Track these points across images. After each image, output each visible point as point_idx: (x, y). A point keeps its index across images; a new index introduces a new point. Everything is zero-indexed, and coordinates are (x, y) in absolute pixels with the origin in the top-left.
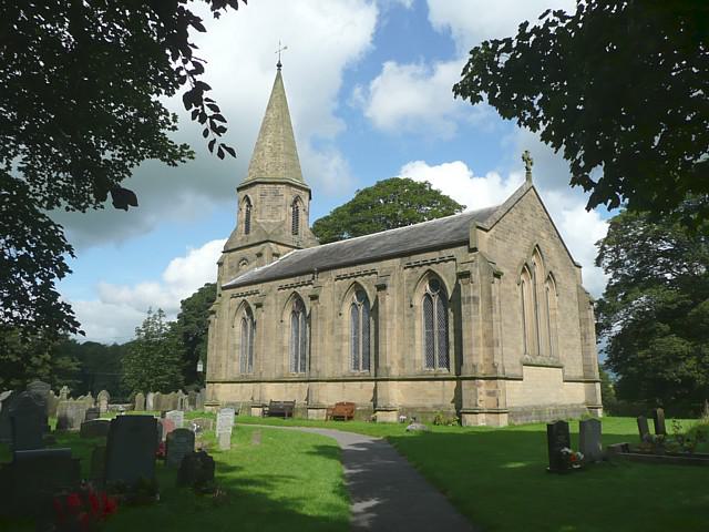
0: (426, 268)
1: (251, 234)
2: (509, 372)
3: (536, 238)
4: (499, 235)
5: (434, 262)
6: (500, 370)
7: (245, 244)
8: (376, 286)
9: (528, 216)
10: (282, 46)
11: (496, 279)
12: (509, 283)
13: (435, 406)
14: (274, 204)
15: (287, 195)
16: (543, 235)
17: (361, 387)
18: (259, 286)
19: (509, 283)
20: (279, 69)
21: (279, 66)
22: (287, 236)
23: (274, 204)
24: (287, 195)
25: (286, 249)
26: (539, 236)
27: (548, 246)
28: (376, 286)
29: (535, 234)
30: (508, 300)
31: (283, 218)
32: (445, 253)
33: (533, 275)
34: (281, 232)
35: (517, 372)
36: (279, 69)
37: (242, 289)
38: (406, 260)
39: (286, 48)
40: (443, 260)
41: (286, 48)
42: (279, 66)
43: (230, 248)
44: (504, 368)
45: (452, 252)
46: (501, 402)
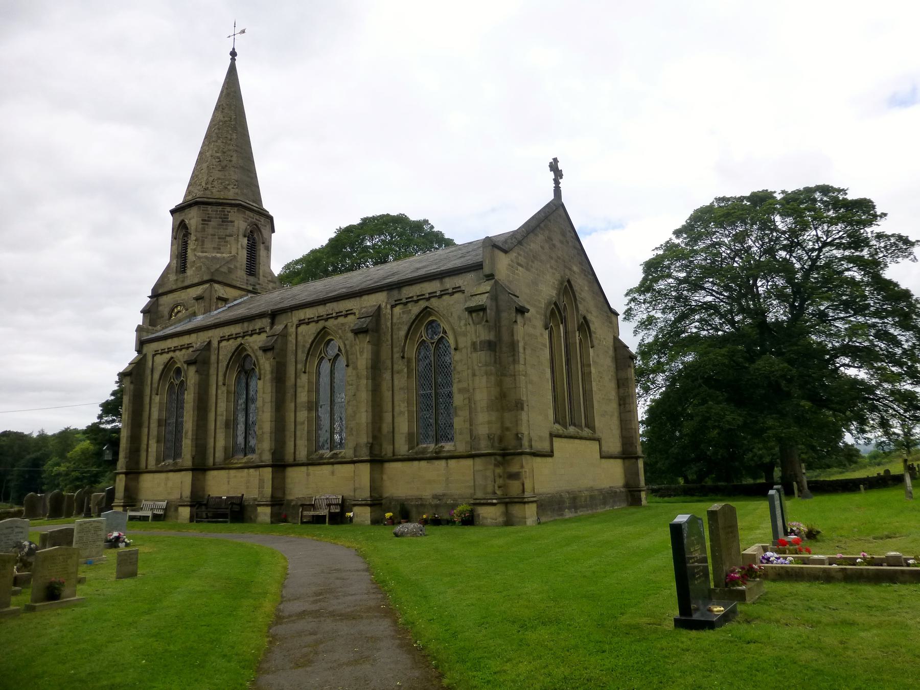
0: (423, 304)
1: (189, 272)
2: (539, 446)
3: (567, 271)
4: (522, 260)
5: (432, 295)
6: (525, 443)
7: (180, 285)
8: (352, 331)
9: (558, 244)
10: (238, 30)
11: (519, 319)
12: (534, 327)
13: (435, 497)
14: (222, 232)
15: (240, 223)
16: (575, 268)
17: (167, 479)
18: (193, 337)
19: (534, 327)
20: (233, 60)
21: (233, 54)
22: (240, 276)
23: (222, 232)
24: (240, 223)
25: (236, 293)
26: (570, 269)
27: (580, 283)
28: (352, 331)
29: (565, 267)
30: (233, 647)
31: (234, 253)
32: (449, 283)
33: (564, 320)
34: (230, 271)
35: (544, 446)
36: (233, 60)
37: (169, 341)
38: (395, 294)
39: (243, 32)
40: (444, 293)
41: (243, 32)
42: (233, 54)
43: (160, 291)
44: (530, 440)
45: (458, 281)
46: (528, 486)
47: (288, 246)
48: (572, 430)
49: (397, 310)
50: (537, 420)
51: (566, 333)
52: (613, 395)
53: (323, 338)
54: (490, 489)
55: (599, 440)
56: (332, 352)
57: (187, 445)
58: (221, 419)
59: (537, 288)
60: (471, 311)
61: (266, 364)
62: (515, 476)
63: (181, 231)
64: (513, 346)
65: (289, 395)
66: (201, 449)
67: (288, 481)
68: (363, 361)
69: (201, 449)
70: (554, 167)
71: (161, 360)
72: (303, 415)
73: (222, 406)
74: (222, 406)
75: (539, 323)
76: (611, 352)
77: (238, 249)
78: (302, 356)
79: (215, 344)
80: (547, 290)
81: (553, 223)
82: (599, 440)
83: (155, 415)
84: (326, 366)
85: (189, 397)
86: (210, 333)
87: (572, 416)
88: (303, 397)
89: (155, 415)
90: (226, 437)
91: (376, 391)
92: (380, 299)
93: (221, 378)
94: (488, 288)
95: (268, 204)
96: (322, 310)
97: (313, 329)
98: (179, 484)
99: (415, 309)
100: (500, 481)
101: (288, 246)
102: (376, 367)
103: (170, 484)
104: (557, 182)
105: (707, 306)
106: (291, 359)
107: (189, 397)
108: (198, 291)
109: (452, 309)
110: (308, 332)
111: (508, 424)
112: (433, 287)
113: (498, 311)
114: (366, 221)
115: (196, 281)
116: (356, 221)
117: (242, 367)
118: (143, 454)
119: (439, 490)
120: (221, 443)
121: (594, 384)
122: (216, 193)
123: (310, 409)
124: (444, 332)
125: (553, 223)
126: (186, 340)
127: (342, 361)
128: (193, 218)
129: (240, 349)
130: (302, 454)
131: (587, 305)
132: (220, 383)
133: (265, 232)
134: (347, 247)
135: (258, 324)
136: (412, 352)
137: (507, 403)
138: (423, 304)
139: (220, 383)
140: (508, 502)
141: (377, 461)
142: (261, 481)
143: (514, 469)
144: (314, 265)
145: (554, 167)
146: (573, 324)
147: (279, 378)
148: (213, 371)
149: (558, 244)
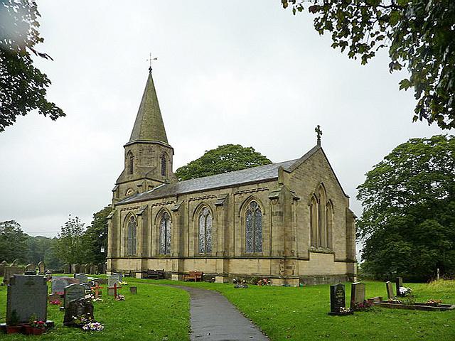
0: (249, 194)
3: (322, 179)
4: (298, 176)
6: (295, 255)
9: (318, 167)
15: (157, 151)
21: (150, 69)
24: (157, 151)
27: (329, 185)
31: (155, 165)
33: (319, 201)
42: (150, 69)
45: (266, 185)
47: (180, 161)
48: (320, 249)
49: (236, 196)
50: (302, 244)
51: (319, 206)
52: (344, 234)
53: (201, 206)
54: (277, 272)
55: (334, 254)
56: (205, 212)
57: (139, 248)
58: (154, 239)
59: (304, 188)
60: (271, 199)
61: (175, 217)
62: (290, 268)
63: (129, 154)
64: (291, 214)
65: (185, 230)
66: (145, 250)
67: (185, 264)
68: (221, 218)
69: (145, 250)
70: (318, 131)
71: (124, 213)
72: (192, 238)
73: (154, 233)
74: (154, 233)
75: (305, 204)
76: (344, 215)
77: (157, 164)
78: (191, 214)
79: (150, 207)
80: (311, 189)
81: (317, 156)
82: (334, 254)
83: (123, 236)
84: (202, 219)
85: (139, 229)
86: (148, 202)
87: (320, 244)
88: (192, 231)
89: (123, 236)
90: (156, 246)
91: (226, 230)
92: (230, 190)
93: (153, 221)
94: (280, 189)
95: (171, 142)
96: (200, 195)
97: (197, 203)
98: (135, 265)
99: (246, 197)
100: (282, 269)
101: (180, 161)
102: (226, 221)
103: (131, 264)
104: (319, 137)
105: (401, 193)
106: (186, 215)
107: (139, 229)
108: (139, 182)
109: (263, 197)
110: (194, 204)
111: (287, 246)
112: (255, 187)
113: (285, 199)
114: (220, 148)
115: (139, 177)
116: (215, 147)
117: (163, 217)
118: (118, 251)
119: (255, 272)
120: (154, 248)
121: (333, 229)
122: (145, 138)
123: (195, 236)
124: (259, 206)
125: (317, 156)
126: (136, 205)
127: (210, 216)
128: (135, 149)
129: (162, 210)
130: (154, 254)
131: (332, 193)
132: (153, 223)
133: (170, 155)
134: (211, 163)
135: (170, 199)
136: (243, 214)
137: (287, 237)
138: (249, 194)
139: (153, 223)
140: (285, 279)
141: (182, 258)
142: (173, 264)
143: (290, 265)
144: (194, 170)
145: (318, 131)
146: (323, 203)
147: (181, 223)
148: (149, 218)
149: (318, 167)
